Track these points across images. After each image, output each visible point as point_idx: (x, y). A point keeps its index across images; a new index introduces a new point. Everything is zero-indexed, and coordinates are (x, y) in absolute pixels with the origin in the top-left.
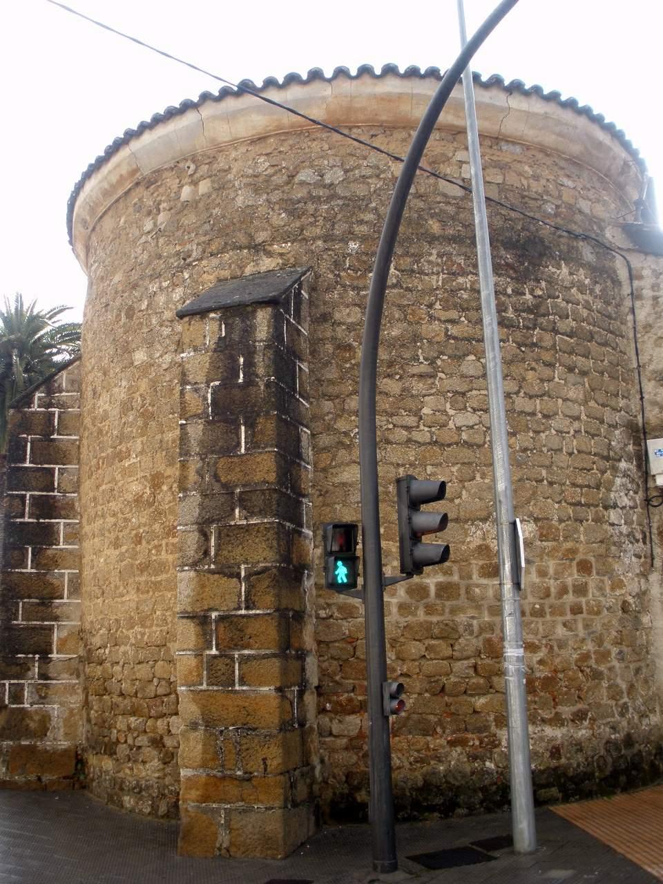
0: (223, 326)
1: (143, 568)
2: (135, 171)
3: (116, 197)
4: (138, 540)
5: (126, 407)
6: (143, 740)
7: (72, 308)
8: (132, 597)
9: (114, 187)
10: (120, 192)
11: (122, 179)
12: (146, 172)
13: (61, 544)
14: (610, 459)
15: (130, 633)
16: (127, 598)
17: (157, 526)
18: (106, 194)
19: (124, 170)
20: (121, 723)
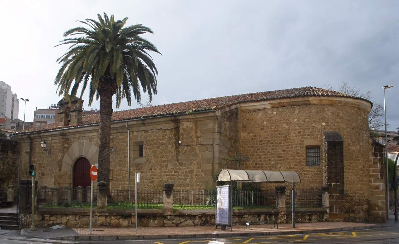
0: (86, 44)
1: (361, 181)
2: (359, 105)
3: (352, 106)
4: (361, 176)
5: (359, 152)
6: (361, 209)
7: (152, 32)
8: (360, 185)
9: (354, 104)
10: (354, 106)
11: (357, 105)
12: (360, 107)
13: (31, 180)
14: (366, 191)
15: (359, 192)
16: (358, 185)
17: (364, 174)
18: (352, 104)
19: (358, 104)
20: (356, 207)
